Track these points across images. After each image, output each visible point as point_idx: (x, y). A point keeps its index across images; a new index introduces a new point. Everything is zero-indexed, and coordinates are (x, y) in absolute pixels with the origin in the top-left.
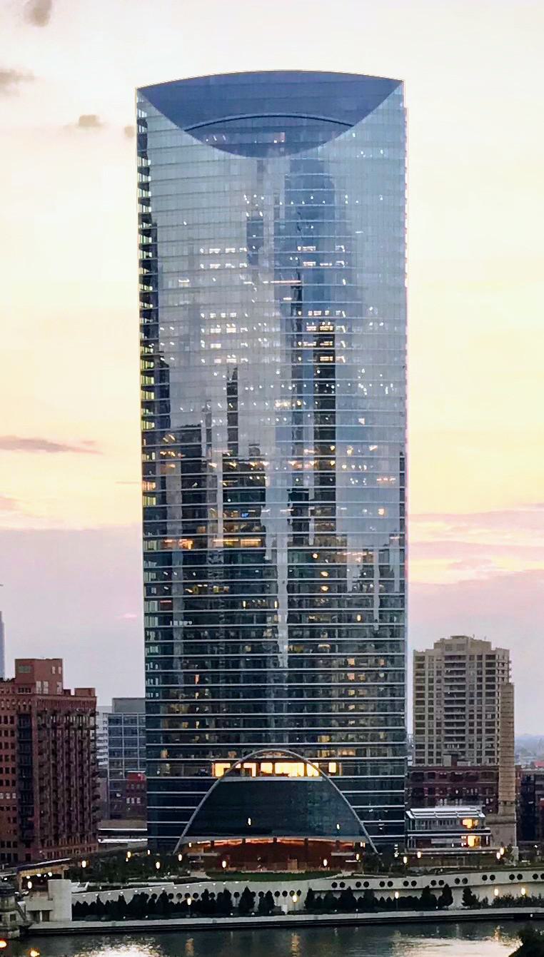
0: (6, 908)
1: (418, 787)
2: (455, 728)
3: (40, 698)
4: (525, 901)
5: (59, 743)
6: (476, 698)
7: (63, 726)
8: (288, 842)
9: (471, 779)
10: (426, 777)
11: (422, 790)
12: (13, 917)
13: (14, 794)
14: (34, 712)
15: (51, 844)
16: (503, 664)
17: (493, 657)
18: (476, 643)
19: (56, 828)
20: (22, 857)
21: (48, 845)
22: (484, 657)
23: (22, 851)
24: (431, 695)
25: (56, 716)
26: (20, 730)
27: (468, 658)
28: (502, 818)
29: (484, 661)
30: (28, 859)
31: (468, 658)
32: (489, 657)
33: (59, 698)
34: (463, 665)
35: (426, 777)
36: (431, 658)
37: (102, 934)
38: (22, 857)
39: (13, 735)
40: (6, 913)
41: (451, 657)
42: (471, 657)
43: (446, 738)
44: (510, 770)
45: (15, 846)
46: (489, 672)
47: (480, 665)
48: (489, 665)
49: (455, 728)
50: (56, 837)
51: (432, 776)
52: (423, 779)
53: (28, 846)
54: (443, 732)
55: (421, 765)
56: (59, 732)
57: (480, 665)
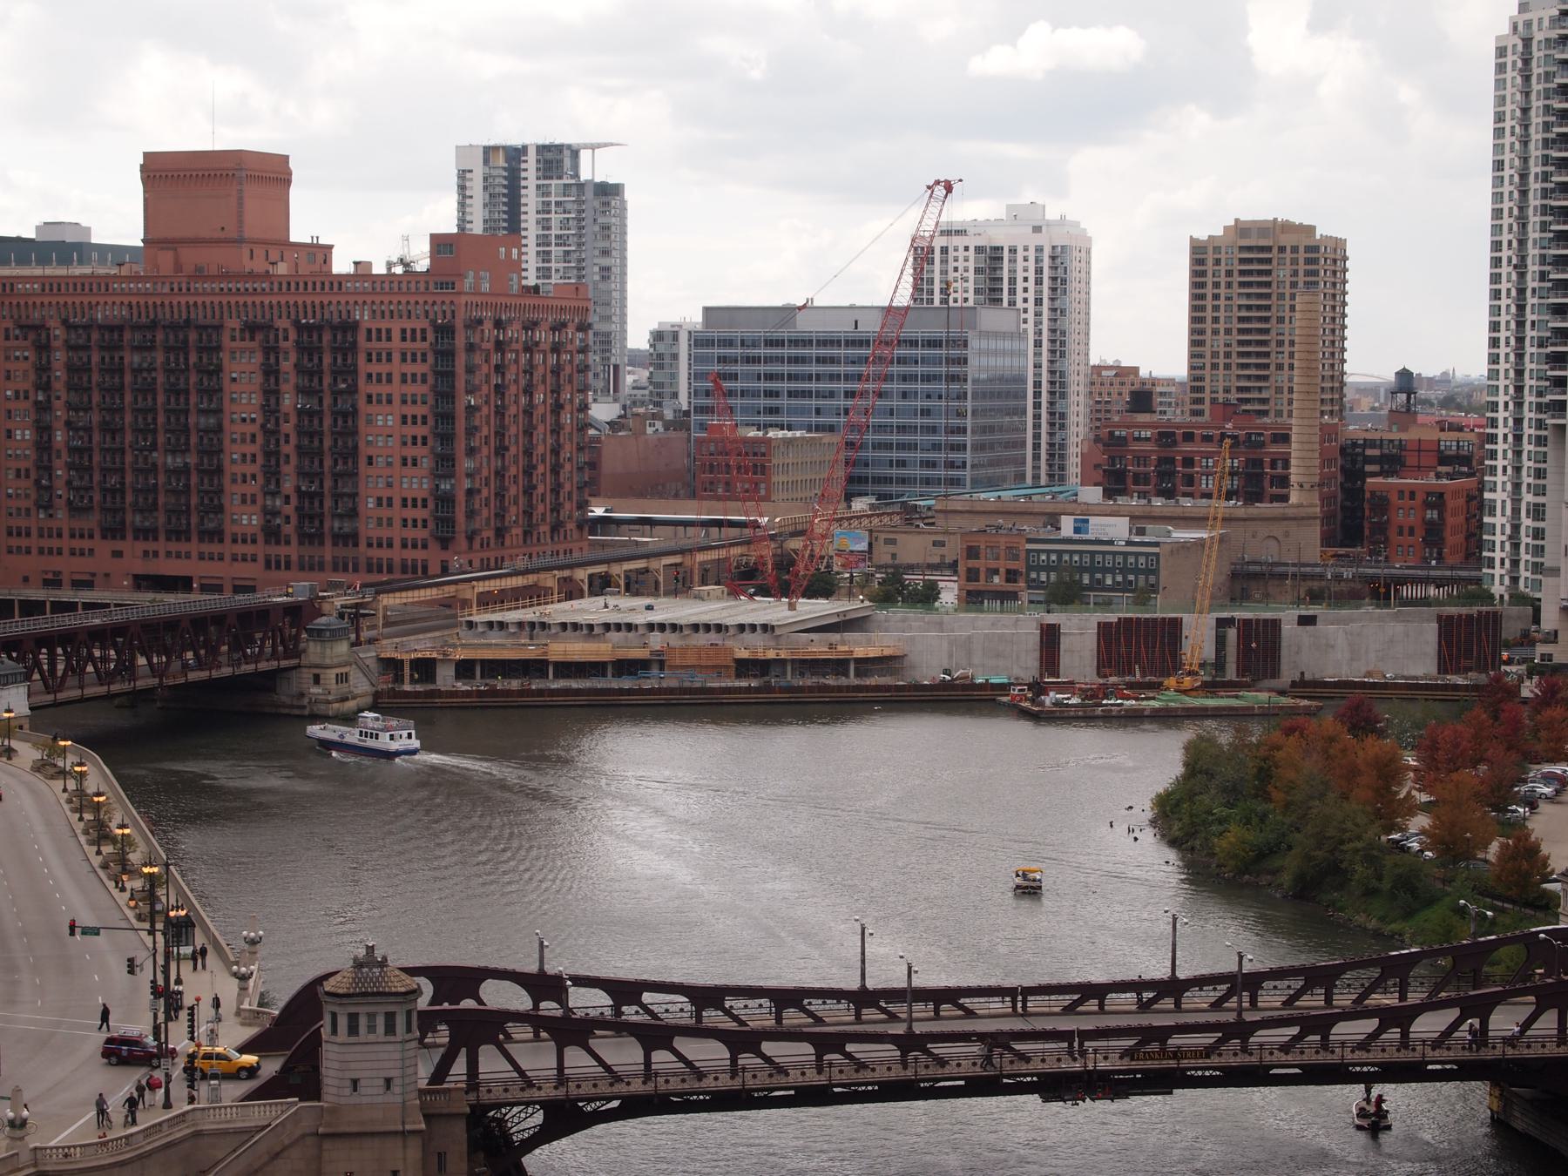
0: (328, 661)
1: (1254, 457)
2: (1253, 361)
3: (469, 299)
4: (671, 691)
5: (537, 375)
6: (1223, 280)
7: (519, 347)
8: (1053, 997)
9: (1464, 457)
10: (1179, 438)
11: (1172, 461)
12: (342, 678)
13: (27, 432)
14: (459, 323)
15: (488, 544)
16: (1335, 261)
17: (1315, 249)
18: (1287, 227)
19: (500, 516)
20: (434, 568)
21: (482, 545)
22: (1302, 250)
23: (433, 556)
24: (1216, 308)
25: (504, 329)
26: (436, 352)
27: (1275, 250)
28: (1295, 510)
29: (1302, 255)
30: (445, 570)
31: (1275, 250)
32: (1309, 249)
33: (513, 301)
34: (1269, 261)
35: (1179, 438)
36: (1217, 249)
37: (1208, 717)
38: (434, 568)
39: (424, 360)
40: (328, 671)
41: (1250, 249)
42: (1282, 249)
43: (1238, 376)
44: (1300, 422)
45: (425, 546)
46: (1308, 273)
47: (1294, 261)
48: (1308, 261)
49: (1253, 361)
50: (500, 533)
51: (1189, 437)
52: (1175, 443)
53: (445, 548)
54: (1234, 367)
55: (1199, 419)
56: (510, 356)
57: (1294, 261)
